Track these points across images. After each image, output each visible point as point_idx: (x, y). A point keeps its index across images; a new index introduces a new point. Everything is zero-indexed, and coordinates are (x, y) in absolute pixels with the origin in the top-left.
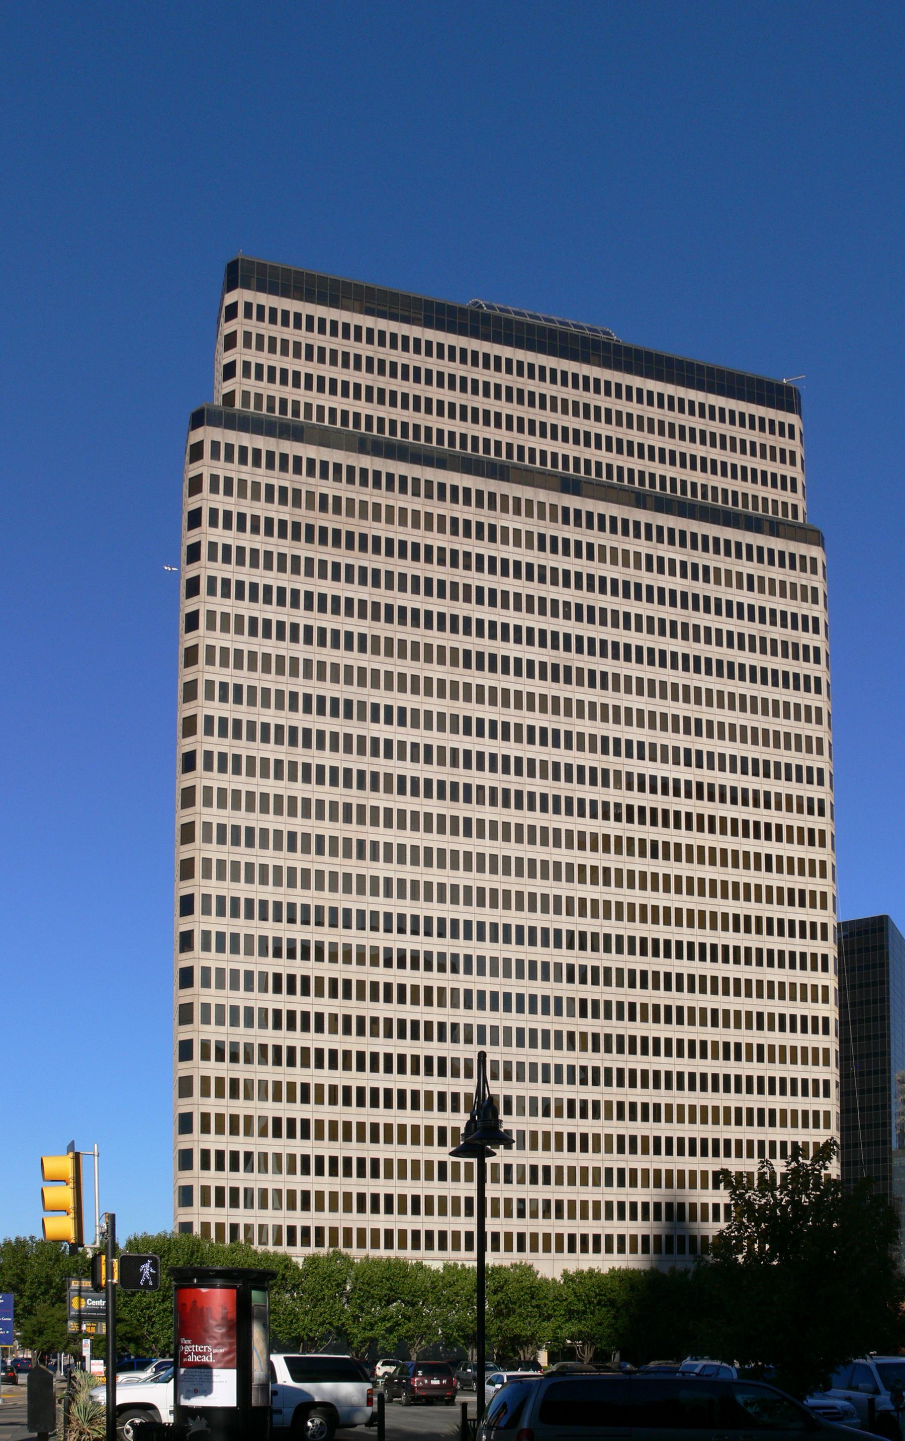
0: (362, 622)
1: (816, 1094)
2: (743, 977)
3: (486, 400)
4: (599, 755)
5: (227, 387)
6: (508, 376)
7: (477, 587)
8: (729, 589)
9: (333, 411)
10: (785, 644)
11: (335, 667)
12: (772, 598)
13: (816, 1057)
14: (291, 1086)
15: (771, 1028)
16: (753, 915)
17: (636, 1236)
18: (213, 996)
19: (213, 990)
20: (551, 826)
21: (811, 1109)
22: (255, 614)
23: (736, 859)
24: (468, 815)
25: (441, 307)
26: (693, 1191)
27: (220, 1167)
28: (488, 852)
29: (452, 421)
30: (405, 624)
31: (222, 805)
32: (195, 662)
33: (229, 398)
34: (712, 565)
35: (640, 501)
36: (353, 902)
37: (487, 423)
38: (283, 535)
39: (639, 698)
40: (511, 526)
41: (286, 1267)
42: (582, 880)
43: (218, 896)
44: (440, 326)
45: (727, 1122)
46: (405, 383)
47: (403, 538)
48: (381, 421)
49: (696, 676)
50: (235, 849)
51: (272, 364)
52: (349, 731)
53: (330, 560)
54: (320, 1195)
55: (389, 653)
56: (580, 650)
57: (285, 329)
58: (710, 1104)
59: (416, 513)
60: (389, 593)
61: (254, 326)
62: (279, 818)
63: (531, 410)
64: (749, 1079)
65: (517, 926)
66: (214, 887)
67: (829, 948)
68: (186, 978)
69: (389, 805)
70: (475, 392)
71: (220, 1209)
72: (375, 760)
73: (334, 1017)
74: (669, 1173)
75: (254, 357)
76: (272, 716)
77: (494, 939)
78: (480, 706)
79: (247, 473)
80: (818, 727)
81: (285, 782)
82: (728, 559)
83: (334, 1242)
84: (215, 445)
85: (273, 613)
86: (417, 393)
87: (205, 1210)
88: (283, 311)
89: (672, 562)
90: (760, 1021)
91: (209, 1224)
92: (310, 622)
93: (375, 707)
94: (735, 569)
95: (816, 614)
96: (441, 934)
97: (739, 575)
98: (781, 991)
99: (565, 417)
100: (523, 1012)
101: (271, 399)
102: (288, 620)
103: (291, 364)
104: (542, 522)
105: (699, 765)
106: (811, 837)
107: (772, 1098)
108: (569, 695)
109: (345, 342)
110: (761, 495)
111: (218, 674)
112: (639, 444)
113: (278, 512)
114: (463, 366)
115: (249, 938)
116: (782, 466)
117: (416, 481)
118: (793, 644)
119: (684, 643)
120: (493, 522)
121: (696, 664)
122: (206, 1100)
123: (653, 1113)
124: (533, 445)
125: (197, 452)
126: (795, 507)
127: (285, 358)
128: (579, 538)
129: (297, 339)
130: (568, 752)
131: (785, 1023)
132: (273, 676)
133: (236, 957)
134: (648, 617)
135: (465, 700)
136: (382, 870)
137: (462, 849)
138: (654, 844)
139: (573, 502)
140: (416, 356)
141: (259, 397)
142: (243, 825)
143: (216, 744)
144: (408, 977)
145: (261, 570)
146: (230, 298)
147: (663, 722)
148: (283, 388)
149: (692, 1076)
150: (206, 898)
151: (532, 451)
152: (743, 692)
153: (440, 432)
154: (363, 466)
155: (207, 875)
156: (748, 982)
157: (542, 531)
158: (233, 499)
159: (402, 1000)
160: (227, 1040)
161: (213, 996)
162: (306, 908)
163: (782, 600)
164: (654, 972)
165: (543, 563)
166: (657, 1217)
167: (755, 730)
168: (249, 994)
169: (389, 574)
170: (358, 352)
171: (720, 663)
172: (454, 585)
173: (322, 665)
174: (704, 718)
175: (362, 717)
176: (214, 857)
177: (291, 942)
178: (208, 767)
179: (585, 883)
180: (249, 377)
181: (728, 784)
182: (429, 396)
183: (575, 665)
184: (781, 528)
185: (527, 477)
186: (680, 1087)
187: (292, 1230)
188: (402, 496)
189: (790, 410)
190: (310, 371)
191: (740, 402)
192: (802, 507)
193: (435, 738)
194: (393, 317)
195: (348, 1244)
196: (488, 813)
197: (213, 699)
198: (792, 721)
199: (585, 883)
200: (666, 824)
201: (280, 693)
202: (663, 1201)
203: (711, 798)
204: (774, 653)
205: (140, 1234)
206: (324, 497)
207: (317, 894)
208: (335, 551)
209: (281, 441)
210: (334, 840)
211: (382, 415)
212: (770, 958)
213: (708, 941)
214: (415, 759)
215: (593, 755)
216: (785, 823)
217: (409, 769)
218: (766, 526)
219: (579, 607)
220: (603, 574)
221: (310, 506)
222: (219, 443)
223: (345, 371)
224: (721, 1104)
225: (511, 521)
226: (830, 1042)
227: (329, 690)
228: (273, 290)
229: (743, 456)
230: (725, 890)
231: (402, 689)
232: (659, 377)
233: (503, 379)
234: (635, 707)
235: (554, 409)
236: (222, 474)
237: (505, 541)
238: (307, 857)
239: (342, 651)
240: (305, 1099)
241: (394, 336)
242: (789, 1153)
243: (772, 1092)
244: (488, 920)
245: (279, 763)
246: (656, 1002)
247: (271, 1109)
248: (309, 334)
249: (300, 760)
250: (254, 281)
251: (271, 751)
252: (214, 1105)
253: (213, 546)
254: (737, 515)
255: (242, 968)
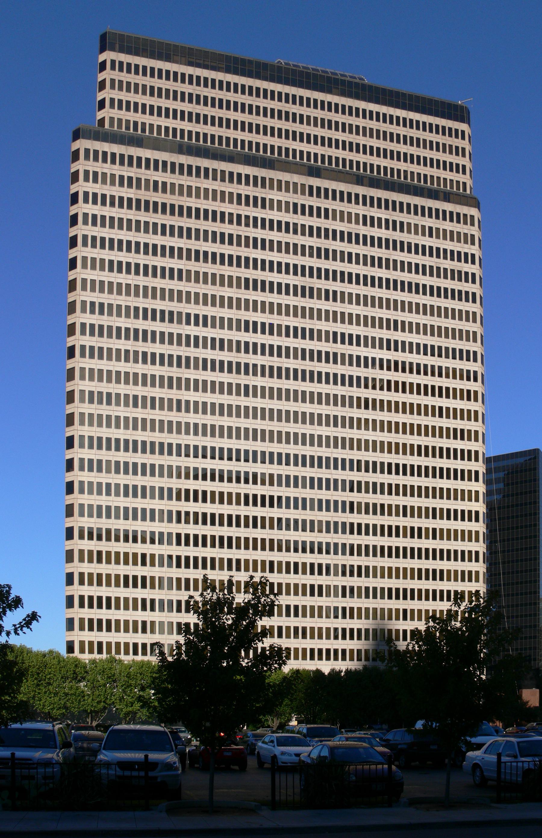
0: (180, 261)
1: (470, 560)
2: (423, 485)
3: (265, 119)
4: (331, 344)
5: (100, 115)
6: (279, 103)
7: (254, 238)
8: (416, 237)
9: (167, 128)
10: (453, 271)
11: (163, 290)
12: (445, 242)
13: (470, 536)
14: (135, 555)
15: (441, 518)
16: (430, 445)
17: (353, 650)
18: (86, 499)
19: (86, 495)
20: (300, 389)
21: (467, 570)
22: (112, 258)
23: (419, 410)
24: (247, 383)
25: (236, 60)
26: (390, 621)
27: (91, 606)
28: (340, 414)
29: (243, 133)
30: (207, 262)
31: (91, 379)
32: (75, 289)
33: (102, 122)
34: (405, 221)
35: (359, 180)
36: (174, 439)
37: (337, 147)
38: (130, 207)
39: (357, 307)
40: (276, 198)
41: (76, 666)
42: (367, 428)
43: (89, 436)
44: (236, 72)
45: (412, 578)
46: (213, 109)
47: (206, 207)
48: (198, 134)
49: (395, 292)
50: (100, 406)
51: (144, 102)
52: (171, 331)
53: (160, 222)
54: (118, 622)
55: (197, 281)
56: (319, 277)
57: (137, 76)
58: (401, 566)
59: (214, 191)
60: (197, 242)
61: (116, 75)
62: (127, 387)
63: (294, 124)
64: (427, 550)
65: (278, 453)
66: (86, 431)
67: (480, 467)
68: (70, 488)
69: (197, 377)
70: (258, 114)
71: (91, 633)
72: (188, 349)
73: (162, 512)
74: (375, 610)
75: (117, 95)
76: (123, 322)
77: (312, 466)
78: (287, 318)
79: (107, 168)
80: (474, 324)
81: (131, 364)
82: (416, 217)
83: (109, 651)
84: (87, 151)
85: (124, 257)
86: (221, 116)
87: (82, 633)
88: (234, 83)
89: (380, 219)
90: (434, 513)
91: (120, 643)
92: (147, 262)
93: (188, 315)
94: (420, 223)
95: (473, 252)
96: (367, 470)
97: (423, 227)
98: (448, 494)
99: (316, 129)
100: (391, 515)
101: (128, 122)
102: (133, 261)
103: (209, 111)
104: (295, 196)
105: (396, 350)
106: (469, 395)
107: (441, 562)
108: (312, 306)
109: (175, 84)
110: (442, 176)
111: (89, 296)
112: (404, 153)
113: (127, 193)
114: (250, 98)
115: (108, 462)
116: (457, 157)
117: (215, 171)
118: (458, 271)
119: (387, 271)
120: (264, 196)
121: (395, 285)
122: (82, 564)
123: (361, 571)
124: (295, 147)
125: (75, 156)
126: (464, 184)
127: (136, 95)
128: (319, 205)
129: (144, 83)
130: (312, 342)
131: (450, 515)
132: (123, 297)
133: (100, 474)
134: (408, 263)
135: (356, 325)
136: (192, 418)
137: (355, 416)
138: (367, 400)
139: (315, 182)
140: (220, 92)
141: (120, 120)
142: (105, 391)
143: (88, 341)
144: (209, 486)
145: (116, 230)
146: (102, 58)
147: (373, 322)
148: (136, 114)
149: (434, 550)
150: (82, 437)
151: (294, 151)
152: (425, 302)
153: (235, 140)
154: (181, 162)
155: (82, 423)
156: (427, 488)
157: (296, 201)
158: (98, 185)
159: (204, 500)
160: (95, 526)
161: (86, 499)
162: (247, 452)
163: (451, 243)
164: (411, 486)
165: (296, 221)
166: (367, 638)
167: (461, 331)
168: (109, 498)
169: (295, 245)
170: (183, 90)
171: (410, 284)
172: (239, 237)
173: (154, 289)
174: (400, 319)
175: (180, 322)
176: (87, 412)
177: (204, 470)
178: (83, 355)
179: (322, 425)
180: (114, 108)
181: (415, 362)
182: (228, 117)
183: (316, 286)
184: (451, 196)
185: (286, 167)
186: (397, 556)
187: (135, 645)
188: (206, 181)
189: (463, 121)
190: (152, 103)
191: (430, 117)
192: (469, 183)
193: (226, 334)
194: (206, 67)
195: (118, 652)
196: (259, 381)
197: (86, 312)
198: (457, 321)
199: (322, 425)
200: (440, 396)
201: (128, 308)
202: (371, 628)
203: (404, 371)
204: (446, 277)
205: (28, 646)
206: (156, 183)
207: (151, 434)
208: (163, 216)
209: (129, 147)
210: (263, 410)
211: (198, 130)
212: (441, 473)
213: (401, 462)
214: (213, 347)
215: (327, 344)
216: (451, 386)
217: (209, 354)
218: (441, 195)
219: (319, 249)
220: (335, 228)
221: (147, 188)
222: (89, 150)
223: (175, 102)
224: (409, 566)
225: (275, 195)
226: (480, 527)
227: (159, 305)
228: (129, 52)
229: (431, 152)
230: (412, 429)
231: (205, 303)
232: (377, 102)
233: (276, 105)
234: (354, 312)
235: (309, 124)
236: (91, 169)
237: (271, 208)
238: (196, 416)
239: (167, 280)
240: (144, 564)
241: (265, 91)
242: (452, 597)
243: (442, 559)
244: (308, 454)
245: (127, 352)
246: (367, 501)
247: (340, 581)
248: (152, 79)
249: (141, 350)
250: (117, 46)
251: (123, 344)
252: (87, 568)
253: (86, 215)
254: (422, 189)
255: (104, 481)
